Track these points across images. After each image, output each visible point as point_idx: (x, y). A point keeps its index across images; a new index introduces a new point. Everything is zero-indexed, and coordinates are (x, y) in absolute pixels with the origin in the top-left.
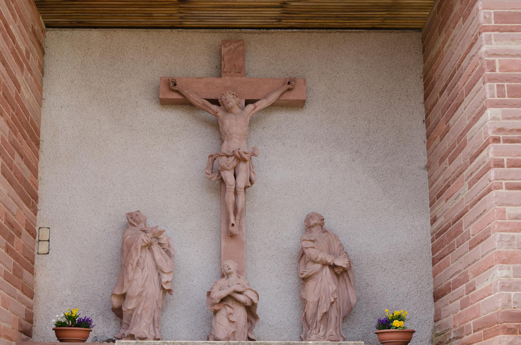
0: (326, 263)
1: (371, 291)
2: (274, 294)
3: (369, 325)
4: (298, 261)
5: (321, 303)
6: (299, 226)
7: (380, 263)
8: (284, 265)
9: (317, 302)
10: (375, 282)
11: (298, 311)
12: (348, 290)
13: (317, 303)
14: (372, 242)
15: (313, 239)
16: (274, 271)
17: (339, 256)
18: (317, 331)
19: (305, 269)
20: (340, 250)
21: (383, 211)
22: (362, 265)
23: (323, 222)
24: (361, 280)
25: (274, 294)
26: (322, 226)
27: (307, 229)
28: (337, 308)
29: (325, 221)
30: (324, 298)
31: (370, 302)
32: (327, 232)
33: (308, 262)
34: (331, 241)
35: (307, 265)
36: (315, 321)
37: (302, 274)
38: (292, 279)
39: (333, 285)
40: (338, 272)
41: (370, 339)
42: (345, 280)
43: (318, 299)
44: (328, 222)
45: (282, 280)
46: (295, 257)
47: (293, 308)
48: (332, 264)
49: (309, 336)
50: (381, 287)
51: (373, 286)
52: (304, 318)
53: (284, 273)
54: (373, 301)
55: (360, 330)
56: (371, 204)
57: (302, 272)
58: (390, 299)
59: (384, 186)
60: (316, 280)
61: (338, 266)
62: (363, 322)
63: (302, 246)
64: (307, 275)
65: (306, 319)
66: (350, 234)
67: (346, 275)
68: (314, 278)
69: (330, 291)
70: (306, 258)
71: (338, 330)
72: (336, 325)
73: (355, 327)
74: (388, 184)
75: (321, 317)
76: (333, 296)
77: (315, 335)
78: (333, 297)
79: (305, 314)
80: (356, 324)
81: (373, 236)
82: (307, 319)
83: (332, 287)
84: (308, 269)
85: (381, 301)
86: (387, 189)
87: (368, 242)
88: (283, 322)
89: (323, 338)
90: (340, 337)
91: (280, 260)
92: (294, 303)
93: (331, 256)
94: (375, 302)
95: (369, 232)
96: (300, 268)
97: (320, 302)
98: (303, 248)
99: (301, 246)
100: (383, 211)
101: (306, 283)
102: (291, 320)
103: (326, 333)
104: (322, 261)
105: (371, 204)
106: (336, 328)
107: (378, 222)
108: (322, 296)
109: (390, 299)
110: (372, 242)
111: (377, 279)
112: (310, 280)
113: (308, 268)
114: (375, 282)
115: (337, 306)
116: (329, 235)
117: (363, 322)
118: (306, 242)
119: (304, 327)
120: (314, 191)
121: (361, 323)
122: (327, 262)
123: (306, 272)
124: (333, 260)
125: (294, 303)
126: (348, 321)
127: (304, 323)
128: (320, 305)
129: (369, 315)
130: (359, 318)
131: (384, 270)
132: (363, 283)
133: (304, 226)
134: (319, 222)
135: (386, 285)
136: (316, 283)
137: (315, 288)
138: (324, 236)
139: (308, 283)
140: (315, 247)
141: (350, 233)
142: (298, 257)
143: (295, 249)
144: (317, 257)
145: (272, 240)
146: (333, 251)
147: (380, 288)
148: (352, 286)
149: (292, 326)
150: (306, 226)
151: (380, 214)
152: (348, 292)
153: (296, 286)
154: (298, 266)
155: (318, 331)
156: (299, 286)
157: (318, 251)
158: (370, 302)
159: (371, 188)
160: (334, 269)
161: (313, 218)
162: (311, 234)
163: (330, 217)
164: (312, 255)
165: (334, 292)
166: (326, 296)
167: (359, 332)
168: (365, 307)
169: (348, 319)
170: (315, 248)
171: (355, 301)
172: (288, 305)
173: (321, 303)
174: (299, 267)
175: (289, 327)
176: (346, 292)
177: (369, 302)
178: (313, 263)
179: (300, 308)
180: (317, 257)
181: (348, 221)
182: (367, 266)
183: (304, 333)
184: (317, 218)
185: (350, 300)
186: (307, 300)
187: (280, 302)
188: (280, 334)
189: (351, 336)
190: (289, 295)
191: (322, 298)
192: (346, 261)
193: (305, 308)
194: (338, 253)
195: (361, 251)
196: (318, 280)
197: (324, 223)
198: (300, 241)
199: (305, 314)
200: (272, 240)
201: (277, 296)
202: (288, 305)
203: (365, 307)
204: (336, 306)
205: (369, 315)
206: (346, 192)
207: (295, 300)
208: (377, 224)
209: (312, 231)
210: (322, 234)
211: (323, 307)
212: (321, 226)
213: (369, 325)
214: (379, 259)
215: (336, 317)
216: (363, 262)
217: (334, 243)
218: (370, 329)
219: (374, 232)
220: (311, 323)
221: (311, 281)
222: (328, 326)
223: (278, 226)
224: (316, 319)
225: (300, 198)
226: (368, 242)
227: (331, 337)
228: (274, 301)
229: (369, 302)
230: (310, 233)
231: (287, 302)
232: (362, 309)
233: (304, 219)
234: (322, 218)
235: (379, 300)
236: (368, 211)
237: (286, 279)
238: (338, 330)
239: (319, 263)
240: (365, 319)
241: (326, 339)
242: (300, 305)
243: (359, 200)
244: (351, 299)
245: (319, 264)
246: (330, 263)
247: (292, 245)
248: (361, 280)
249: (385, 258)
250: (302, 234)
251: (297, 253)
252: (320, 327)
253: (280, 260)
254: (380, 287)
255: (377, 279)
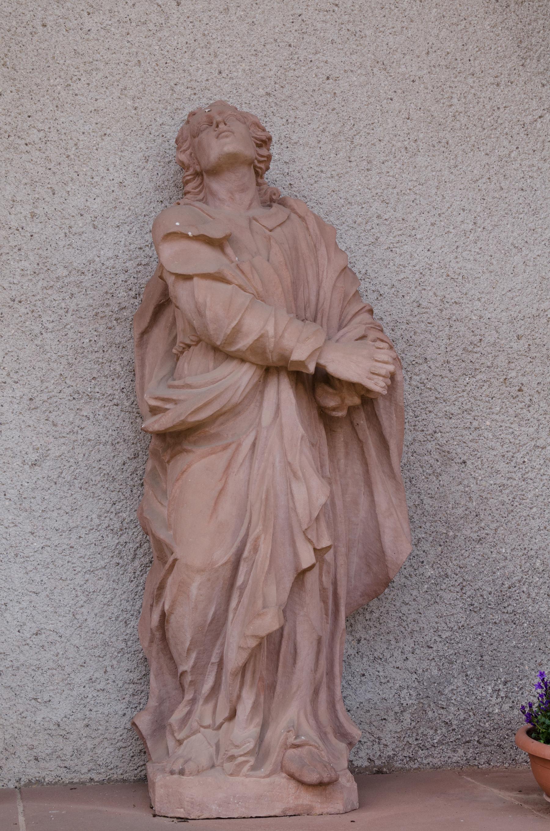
0: (281, 364)
1: (461, 487)
2: (12, 493)
3: (448, 641)
4: (136, 334)
5: (248, 573)
6: (150, 166)
7: (502, 360)
8: (71, 352)
9: (229, 567)
10: (475, 445)
11: (126, 579)
12: (371, 494)
13: (227, 573)
14: (469, 266)
15: (216, 233)
16: (15, 377)
17: (340, 328)
18: (223, 713)
19: (170, 387)
20: (346, 295)
21: (515, 131)
22: (425, 367)
23: (264, 152)
24: (420, 436)
25: (12, 493)
26: (259, 174)
27: (186, 183)
28: (323, 590)
29: (274, 150)
30: (265, 548)
31: (455, 537)
32: (282, 202)
33: (189, 346)
34: (303, 246)
35: (184, 365)
36: (214, 659)
37: (154, 411)
38: (105, 423)
39: (315, 482)
40: (334, 409)
41: (452, 709)
42: (361, 443)
43: (233, 550)
44: (286, 158)
45: (55, 425)
46: (125, 313)
47: (102, 563)
48: (311, 368)
49: (179, 736)
50: (501, 466)
51: (468, 463)
52: (158, 635)
53: (68, 391)
54: (467, 532)
55: (409, 664)
56: (470, 96)
57: (153, 403)
58: (534, 524)
59: (520, 26)
60: (225, 448)
61: (339, 380)
62: (422, 629)
63: (161, 267)
64: (183, 422)
65: (164, 638)
66: (376, 221)
67: (368, 419)
68: (216, 436)
69: (295, 509)
70: (180, 324)
71: (323, 695)
72: (316, 670)
73: (387, 655)
74: (535, 20)
75: (245, 655)
76: (312, 535)
77: (209, 731)
78: (310, 541)
79: (164, 618)
80: (391, 637)
81: (472, 237)
82: (172, 642)
83: (308, 489)
84: (189, 386)
85: (501, 531)
86: (533, 41)
87: (453, 264)
88: (53, 637)
89: (252, 760)
90: (331, 736)
91: (50, 326)
92: (111, 541)
93: (312, 327)
94: (474, 536)
95: (460, 219)
96: (147, 370)
97: (243, 569)
98: (166, 276)
99: (155, 265)
100: (515, 131)
101: (172, 457)
102: (91, 623)
103: (264, 727)
104: (264, 352)
105: (470, 96)
106: (316, 692)
107: (495, 179)
108: (257, 539)
109: (534, 524)
110: (469, 266)
111: (486, 434)
112: (195, 443)
113: (189, 380)
114: (475, 445)
115: (324, 579)
116: (293, 216)
117: (422, 629)
118: (184, 244)
119: (156, 676)
120: (227, 9)
121: (411, 632)
122: (285, 357)
123: (175, 402)
124: (318, 351)
125: (111, 541)
126: (359, 627)
127: (154, 654)
128: (245, 584)
129: (447, 596)
130: (405, 609)
131: (514, 390)
132: (429, 446)
133: (174, 167)
134: (250, 151)
135: (520, 461)
136: (228, 466)
137: (221, 492)
138: (270, 224)
139: (182, 461)
140: (229, 273)
141: (378, 217)
142: (140, 315)
143: (123, 277)
144: (236, 332)
145: (14, 224)
146: (313, 299)
147: (497, 472)
148: (392, 475)
149: (97, 652)
150: (184, 166)
151: (506, 143)
152: (373, 502)
153: (126, 453)
154: (137, 363)
155: (226, 714)
156: (136, 456)
157: (243, 298)
158: (455, 537)
159: (471, 29)
160: (319, 391)
161: (222, 126)
162: (204, 206)
163: (294, 137)
164: (209, 314)
165: (317, 518)
166: (274, 541)
167: (407, 675)
168: (431, 557)
169: (361, 618)
170: (228, 282)
171: (406, 548)
172: (82, 552)
173: (248, 573)
174: (143, 365)
175: (80, 661)
176: (363, 500)
177: (451, 534)
178: (212, 353)
179: (137, 563)
180: (236, 332)
181: (369, 162)
182: (446, 373)
183: (153, 703)
184: (239, 128)
185: (379, 538)
186: (178, 553)
187: (42, 533)
188: (32, 695)
189: (369, 696)
190: (86, 497)
191: (255, 549)
192: (385, 358)
193: (161, 587)
194: (336, 311)
195: (424, 304)
196: (237, 449)
197: (269, 158)
198: (149, 237)
199: (164, 618)
200: (14, 224)
201: (26, 504)
202: (82, 552)
203: (431, 557)
204: (321, 575)
205: (447, 596)
206: (368, 33)
207: (117, 525)
208: (492, 186)
209: (213, 194)
210: (258, 211)
211: (260, 603)
212: (257, 173)
213: (448, 641)
214: (494, 344)
215: (319, 641)
216: (430, 353)
217: (316, 257)
218: (451, 663)
219: (479, 222)
220: (193, 667)
221: (200, 450)
222: (278, 689)
223: (48, 159)
224: (216, 651)
225: (159, 35)
226: (453, 264)
227: (291, 751)
228: (12, 530)
229: (451, 534)
230: (204, 200)
231: (74, 536)
232: (421, 570)
233: (172, 134)
234: (260, 134)
235: (494, 525)
236: (458, 125)
237: (77, 422)
238: (323, 695)
239: (243, 361)
240: (430, 613)
241: (268, 767)
242: (140, 552)
243: (420, 73)
244: (388, 540)
245: (246, 366)
246: (302, 363)
247: (110, 254)
248: (420, 436)
249: (519, 338)
250: (161, 207)
251: (133, 293)
252: (239, 697)
253: (50, 326)
254: (497, 466)
255: (486, 434)
